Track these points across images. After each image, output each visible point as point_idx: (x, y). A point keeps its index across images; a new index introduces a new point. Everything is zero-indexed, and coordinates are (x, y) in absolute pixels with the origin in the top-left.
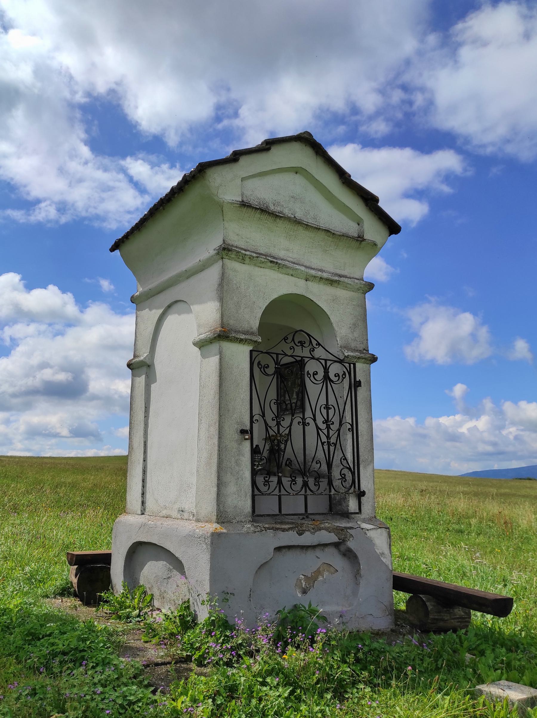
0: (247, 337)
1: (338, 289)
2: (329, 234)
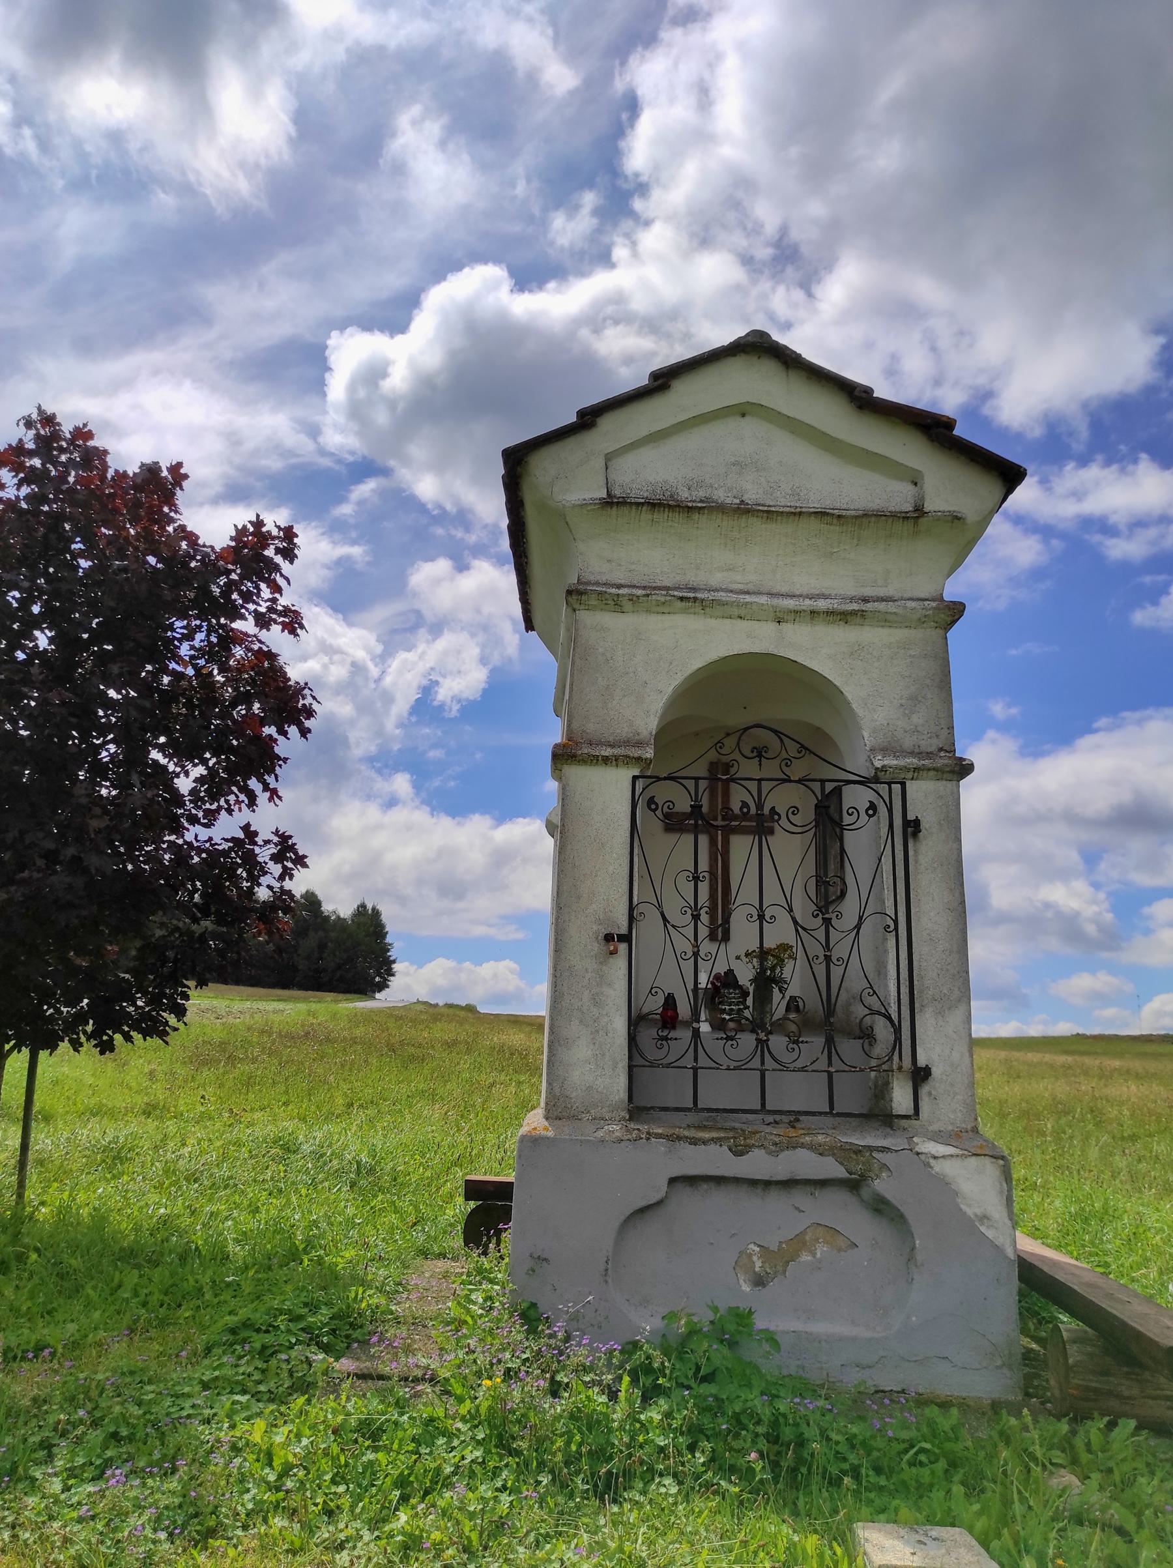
0: (617, 751)
1: (866, 628)
2: (829, 519)
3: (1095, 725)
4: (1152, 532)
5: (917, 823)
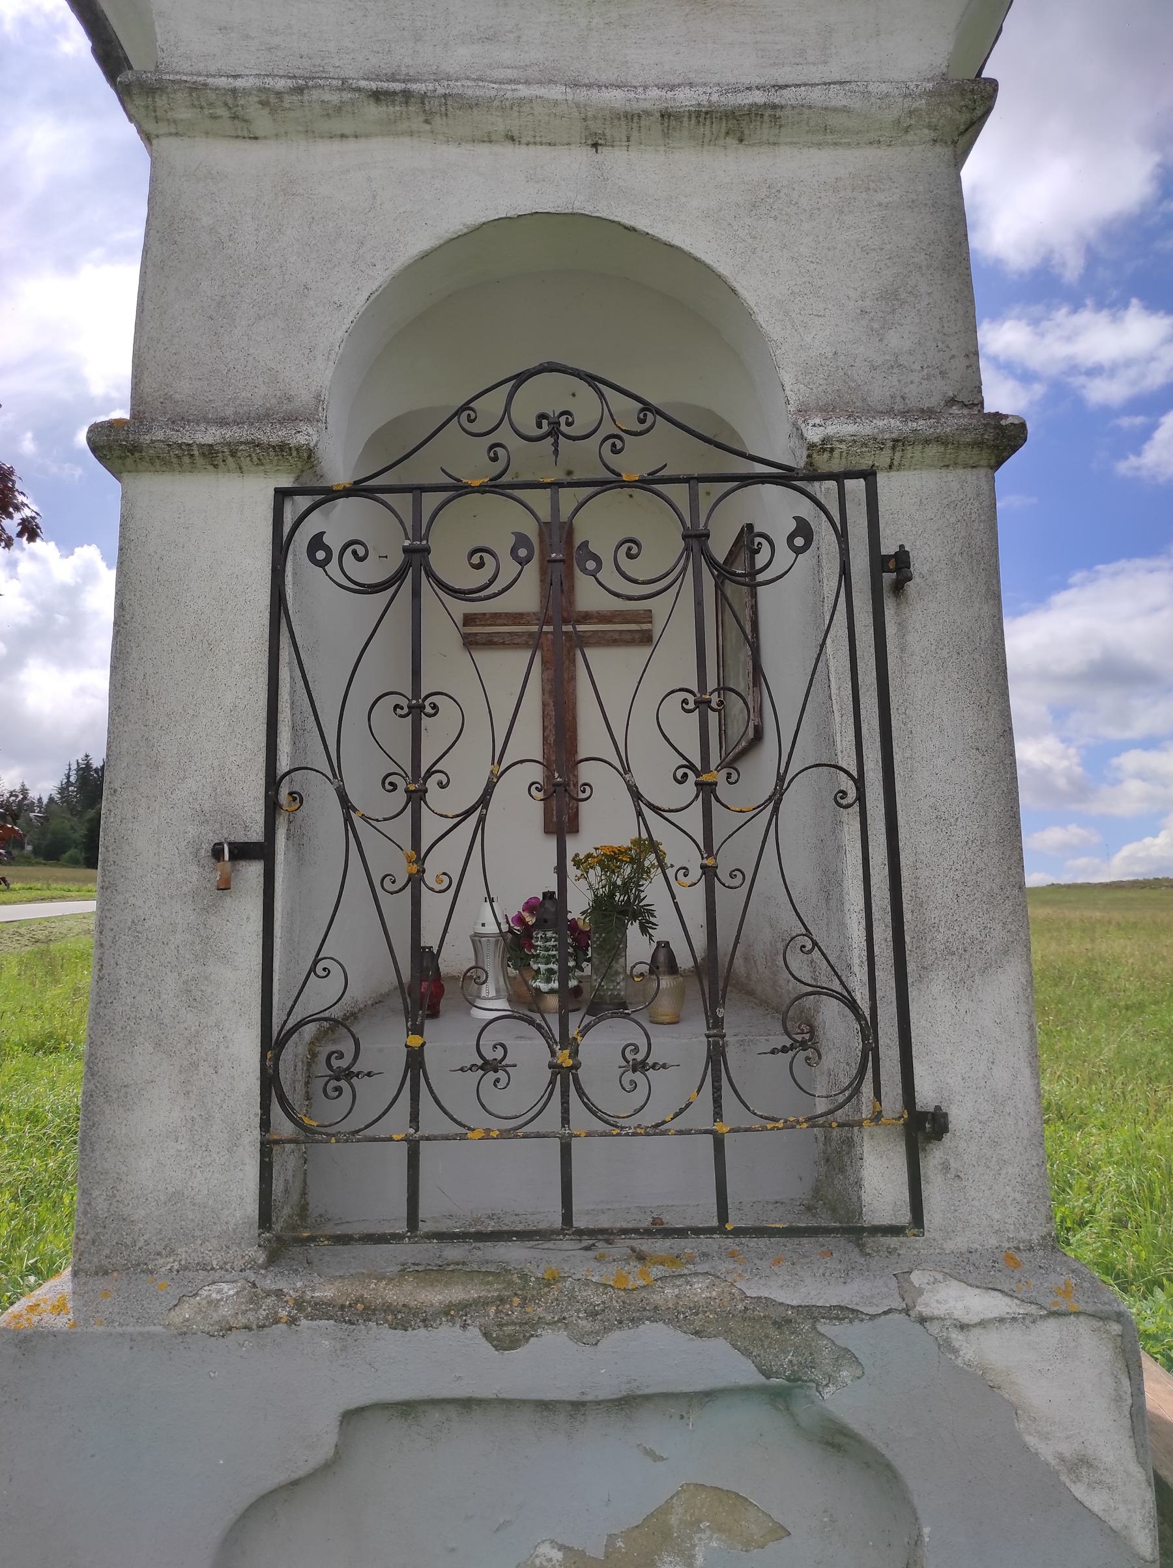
0: (229, 434)
3: (1071, 580)
4: (1132, 373)
5: (902, 560)
